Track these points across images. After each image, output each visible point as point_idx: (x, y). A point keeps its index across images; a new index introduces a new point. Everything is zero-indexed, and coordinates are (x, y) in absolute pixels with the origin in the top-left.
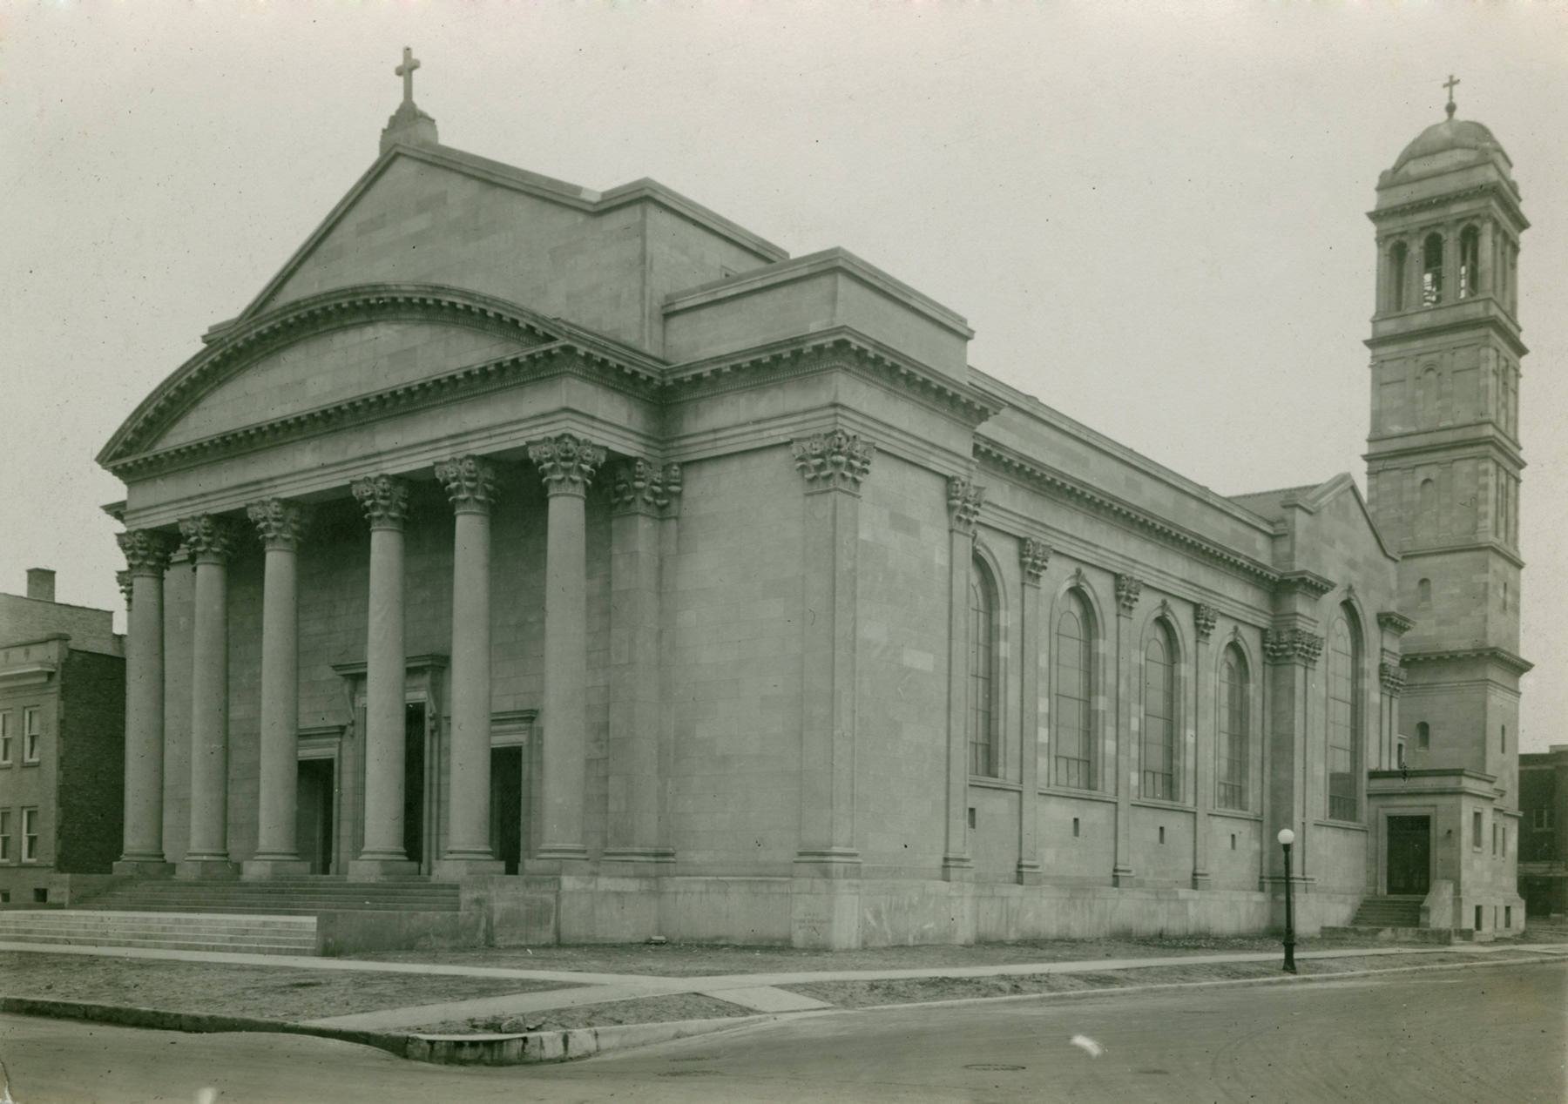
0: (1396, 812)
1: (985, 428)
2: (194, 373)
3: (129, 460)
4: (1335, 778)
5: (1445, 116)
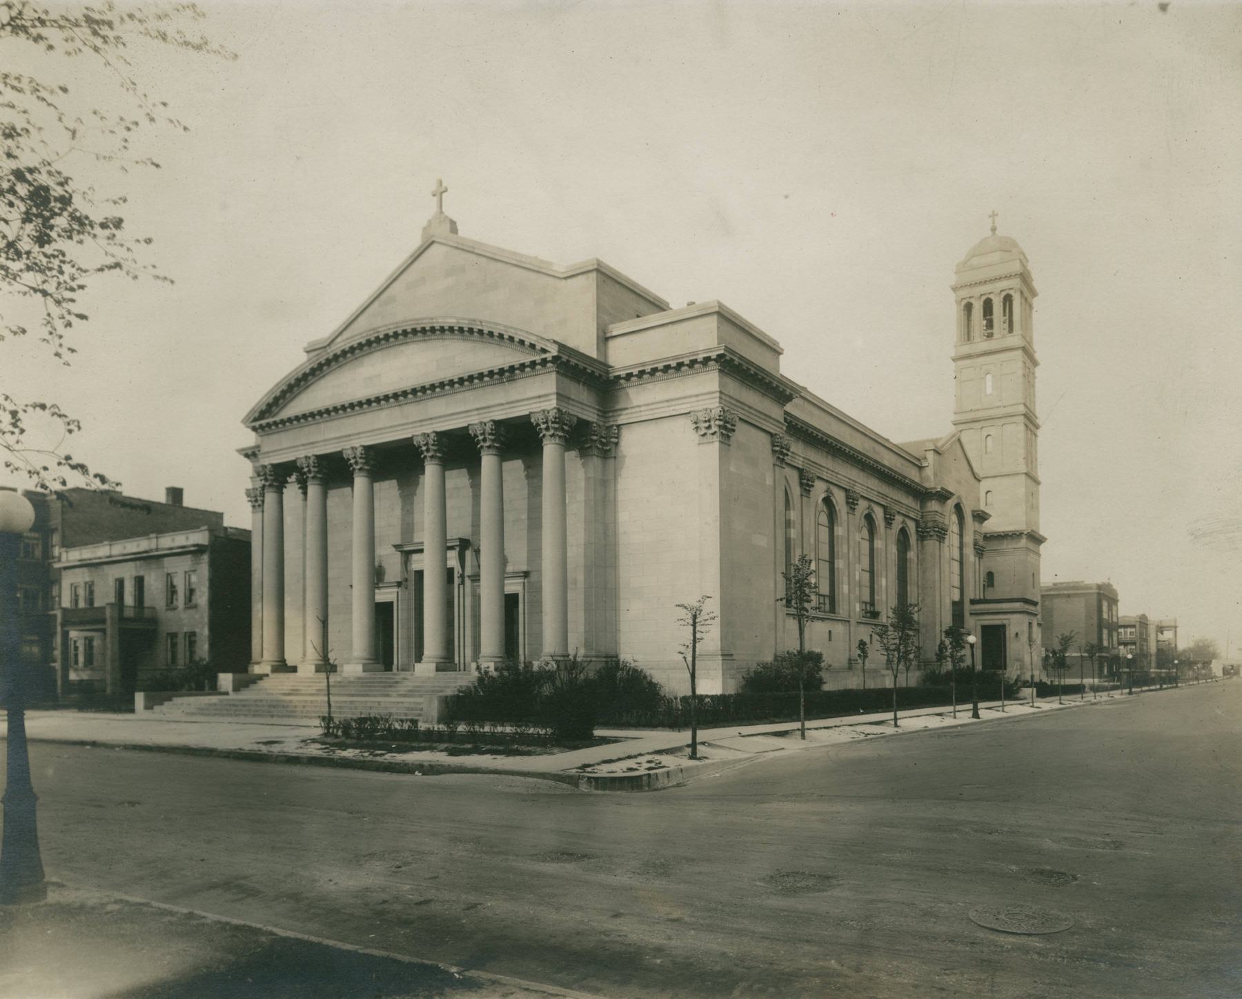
0: (986, 623)
1: (789, 407)
2: (573, 361)
3: (263, 422)
4: (954, 603)
5: (990, 233)
